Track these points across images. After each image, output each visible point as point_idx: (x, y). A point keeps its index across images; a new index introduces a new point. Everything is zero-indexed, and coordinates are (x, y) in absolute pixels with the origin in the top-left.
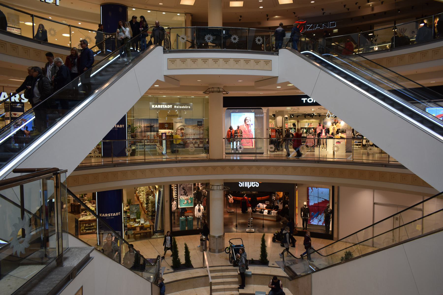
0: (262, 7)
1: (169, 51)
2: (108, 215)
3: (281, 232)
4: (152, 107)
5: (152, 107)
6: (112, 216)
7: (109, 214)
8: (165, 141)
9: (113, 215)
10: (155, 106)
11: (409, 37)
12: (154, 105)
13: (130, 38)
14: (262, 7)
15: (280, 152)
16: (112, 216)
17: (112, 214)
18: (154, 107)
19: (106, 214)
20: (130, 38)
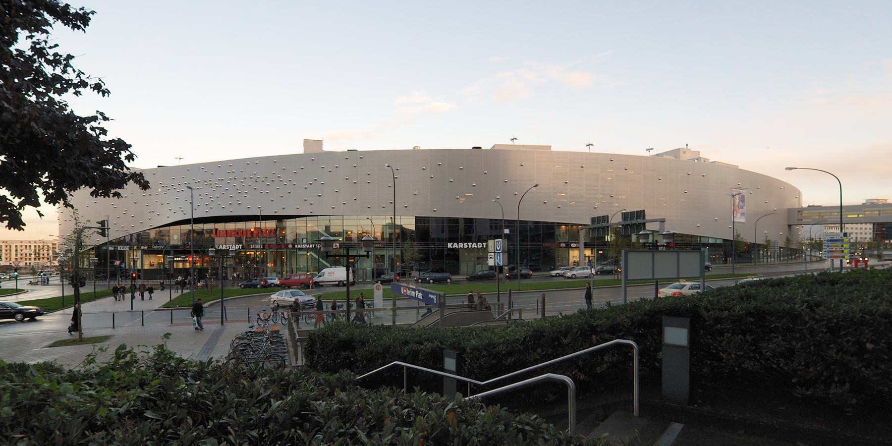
0: (16, 173)
1: (857, 282)
2: (463, 246)
3: (75, 307)
4: (449, 247)
5: (449, 247)
6: (470, 247)
7: (465, 244)
8: (632, 241)
9: (472, 245)
10: (452, 245)
11: (389, 221)
12: (451, 244)
13: (665, 319)
14: (16, 173)
15: (33, 364)
16: (470, 247)
17: (470, 244)
18: (451, 247)
19: (460, 244)
20: (665, 319)
